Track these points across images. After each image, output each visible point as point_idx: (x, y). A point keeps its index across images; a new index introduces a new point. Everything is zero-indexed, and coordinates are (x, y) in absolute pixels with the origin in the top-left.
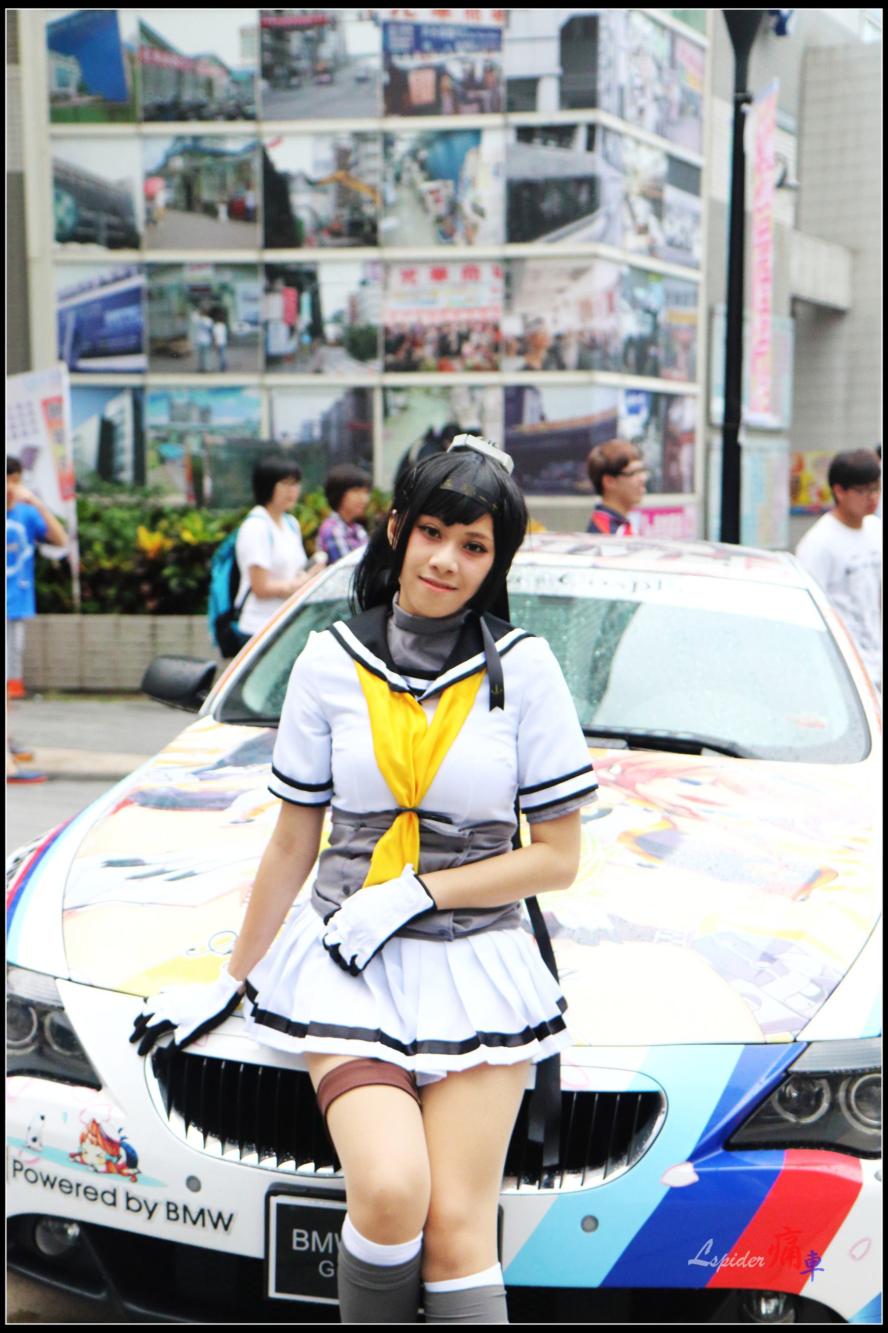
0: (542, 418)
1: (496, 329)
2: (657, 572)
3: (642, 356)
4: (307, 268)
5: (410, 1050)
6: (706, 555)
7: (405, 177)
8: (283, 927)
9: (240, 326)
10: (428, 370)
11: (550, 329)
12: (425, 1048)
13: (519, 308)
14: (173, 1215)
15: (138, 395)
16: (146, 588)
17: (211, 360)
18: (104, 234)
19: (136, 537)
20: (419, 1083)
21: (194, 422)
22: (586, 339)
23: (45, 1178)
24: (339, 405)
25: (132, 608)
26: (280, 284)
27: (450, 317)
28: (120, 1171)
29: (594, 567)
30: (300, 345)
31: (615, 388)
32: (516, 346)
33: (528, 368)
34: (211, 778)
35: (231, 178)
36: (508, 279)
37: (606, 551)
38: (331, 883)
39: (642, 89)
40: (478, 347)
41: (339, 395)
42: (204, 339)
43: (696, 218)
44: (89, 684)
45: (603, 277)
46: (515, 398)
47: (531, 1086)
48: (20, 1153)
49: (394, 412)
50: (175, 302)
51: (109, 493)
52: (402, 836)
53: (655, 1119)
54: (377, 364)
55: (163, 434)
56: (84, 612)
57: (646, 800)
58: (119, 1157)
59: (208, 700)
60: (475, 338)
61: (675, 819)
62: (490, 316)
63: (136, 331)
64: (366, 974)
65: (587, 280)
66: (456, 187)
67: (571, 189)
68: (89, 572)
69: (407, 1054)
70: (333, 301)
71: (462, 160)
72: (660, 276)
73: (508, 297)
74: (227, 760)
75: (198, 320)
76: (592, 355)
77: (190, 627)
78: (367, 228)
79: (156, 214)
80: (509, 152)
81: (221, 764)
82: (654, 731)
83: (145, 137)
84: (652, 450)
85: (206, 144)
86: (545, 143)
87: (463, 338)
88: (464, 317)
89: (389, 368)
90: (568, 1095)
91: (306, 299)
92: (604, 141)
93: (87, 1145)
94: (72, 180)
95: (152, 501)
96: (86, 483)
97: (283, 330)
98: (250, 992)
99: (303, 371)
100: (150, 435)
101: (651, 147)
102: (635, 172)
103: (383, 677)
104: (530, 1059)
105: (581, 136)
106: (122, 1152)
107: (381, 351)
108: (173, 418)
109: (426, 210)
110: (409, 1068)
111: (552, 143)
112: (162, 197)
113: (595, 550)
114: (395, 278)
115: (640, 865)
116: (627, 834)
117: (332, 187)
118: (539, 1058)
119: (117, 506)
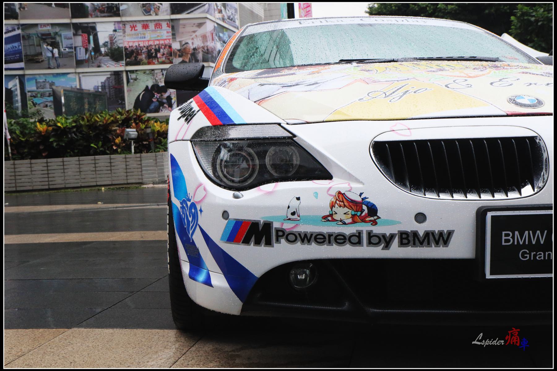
1: (170, 47)
14: (405, 241)
17: (53, 63)
23: (303, 236)
28: (363, 220)
36: (173, 28)
43: (236, 10)
45: (209, 27)
48: (282, 224)
50: (35, 41)
58: (362, 211)
62: (167, 42)
70: (103, 38)
73: (173, 35)
87: (157, 51)
89: (127, 64)
91: (91, 37)
97: (83, 50)
106: (364, 207)
108: (37, 89)
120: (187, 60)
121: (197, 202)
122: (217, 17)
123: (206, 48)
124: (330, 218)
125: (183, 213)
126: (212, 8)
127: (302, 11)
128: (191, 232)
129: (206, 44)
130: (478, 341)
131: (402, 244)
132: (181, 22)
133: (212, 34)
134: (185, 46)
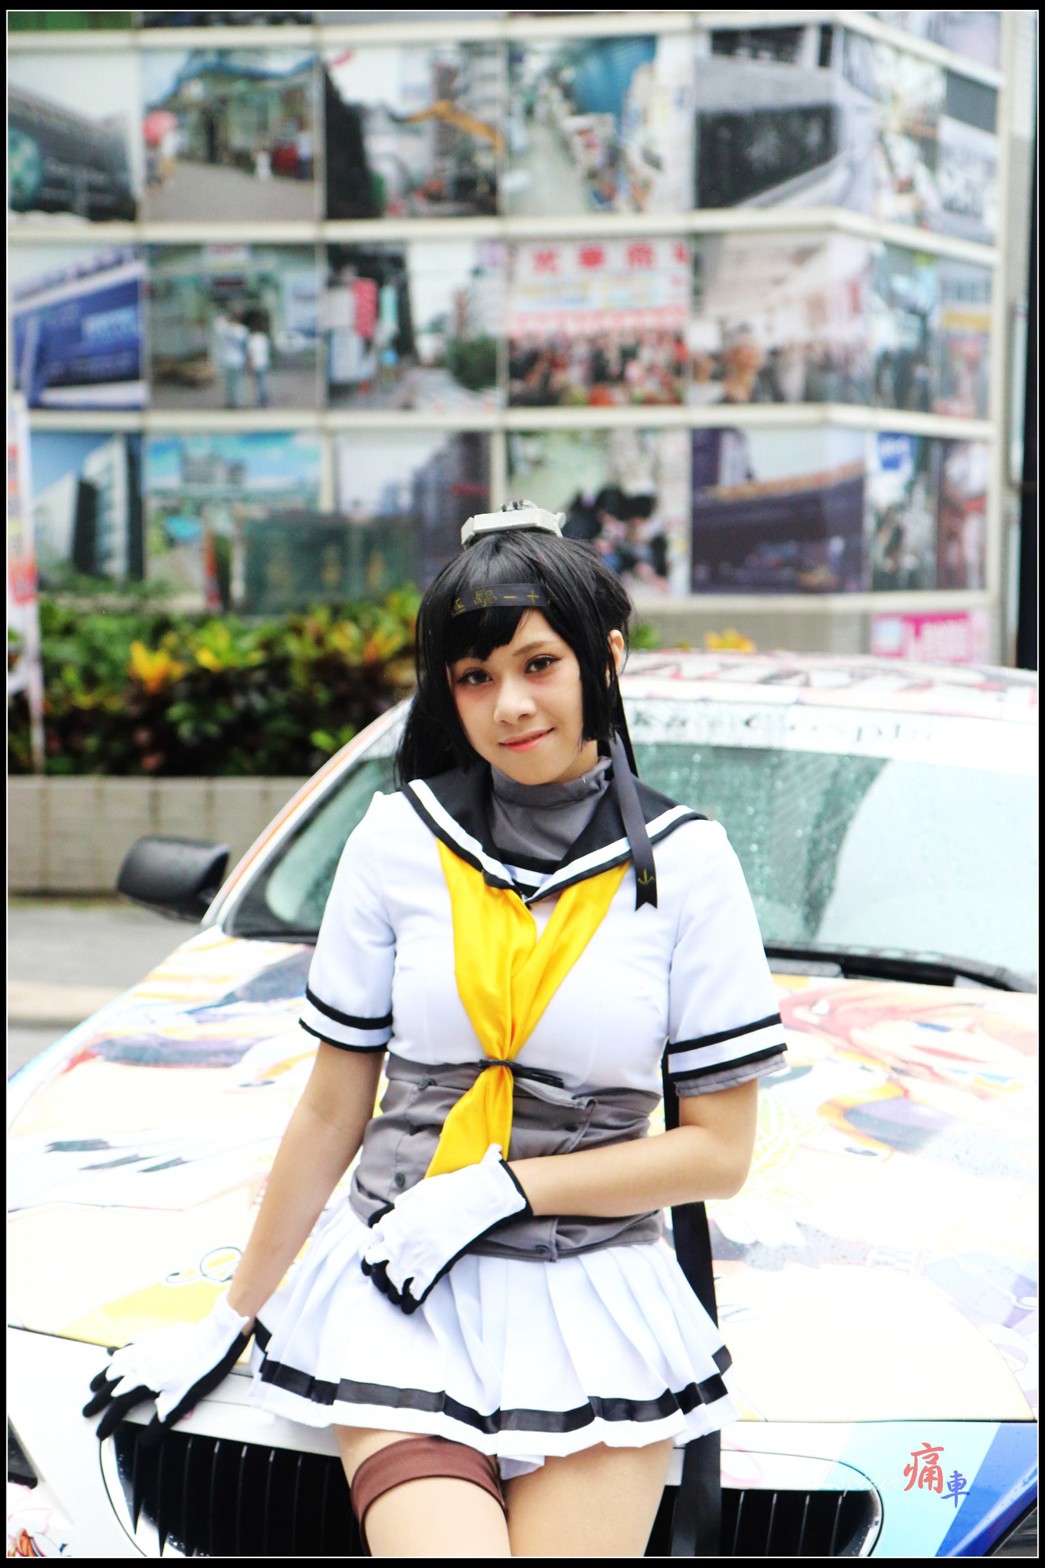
0: (749, 476)
1: (679, 341)
2: (894, 711)
3: (903, 380)
4: (390, 250)
5: (490, 1424)
6: (971, 686)
7: (541, 110)
8: (309, 1240)
9: (290, 337)
10: (574, 403)
11: (762, 340)
12: (513, 1419)
13: (714, 308)
15: (134, 445)
16: (143, 736)
17: (245, 390)
18: (82, 200)
19: (129, 660)
20: (504, 1475)
21: (219, 486)
22: (817, 356)
24: (438, 458)
25: (122, 766)
26: (349, 274)
27: (608, 323)
29: (798, 703)
30: (380, 367)
31: (860, 430)
32: (710, 367)
33: (727, 400)
34: (215, 1019)
35: (275, 114)
36: (697, 265)
37: (816, 679)
38: (378, 1170)
40: (651, 369)
41: (439, 443)
42: (234, 358)
43: (990, 167)
44: (56, 883)
45: (843, 260)
46: (707, 446)
47: (676, 1480)
49: (522, 469)
50: (190, 302)
51: (88, 593)
52: (488, 1101)
53: (865, 1533)
54: (497, 395)
55: (171, 503)
56: (50, 772)
57: (865, 1054)
59: (215, 904)
60: (647, 355)
61: (906, 1081)
62: (669, 322)
63: (132, 346)
64: (428, 1307)
65: (816, 266)
66: (619, 124)
67: (795, 125)
68: (61, 711)
69: (486, 1430)
70: (430, 300)
71: (628, 83)
72: (932, 257)
73: (697, 292)
74: (238, 994)
75: (226, 330)
76: (827, 379)
77: (210, 797)
78: (482, 189)
79: (161, 170)
80: (699, 70)
81: (230, 999)
82: (881, 950)
83: (145, 51)
84: (919, 526)
85: (238, 62)
86: (755, 56)
87: (628, 354)
88: (629, 322)
89: (516, 402)
90: (731, 1494)
91: (389, 297)
92: (846, 50)
94: (34, 117)
95: (155, 606)
96: (55, 577)
98: (261, 1334)
99: (385, 407)
100: (152, 505)
101: (919, 58)
102: (895, 98)
103: (477, 865)
104: (670, 1440)
105: (811, 43)
107: (503, 374)
108: (187, 479)
109: (572, 161)
110: (488, 1453)
111: (766, 55)
112: (171, 142)
113: (800, 678)
114: (525, 263)
115: (849, 1150)
116: (832, 1104)
117: (429, 126)
118: (683, 1440)
119: (102, 611)
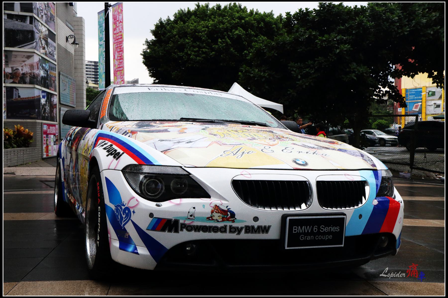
0: (19, 97)
14: (248, 231)
28: (228, 220)
33: (13, 82)
39: (42, 10)
45: (36, 59)
58: (228, 215)
76: (34, 80)
84: (48, 108)
93: (214, 214)
106: (229, 213)
120: (17, 82)
121: (130, 207)
122: (42, 52)
123: (32, 74)
124: (211, 219)
125: (117, 212)
126: (39, 45)
127: (115, 61)
128: (123, 223)
129: (33, 71)
130: (385, 274)
131: (246, 232)
132: (13, 53)
133: (38, 64)
134: (16, 71)
